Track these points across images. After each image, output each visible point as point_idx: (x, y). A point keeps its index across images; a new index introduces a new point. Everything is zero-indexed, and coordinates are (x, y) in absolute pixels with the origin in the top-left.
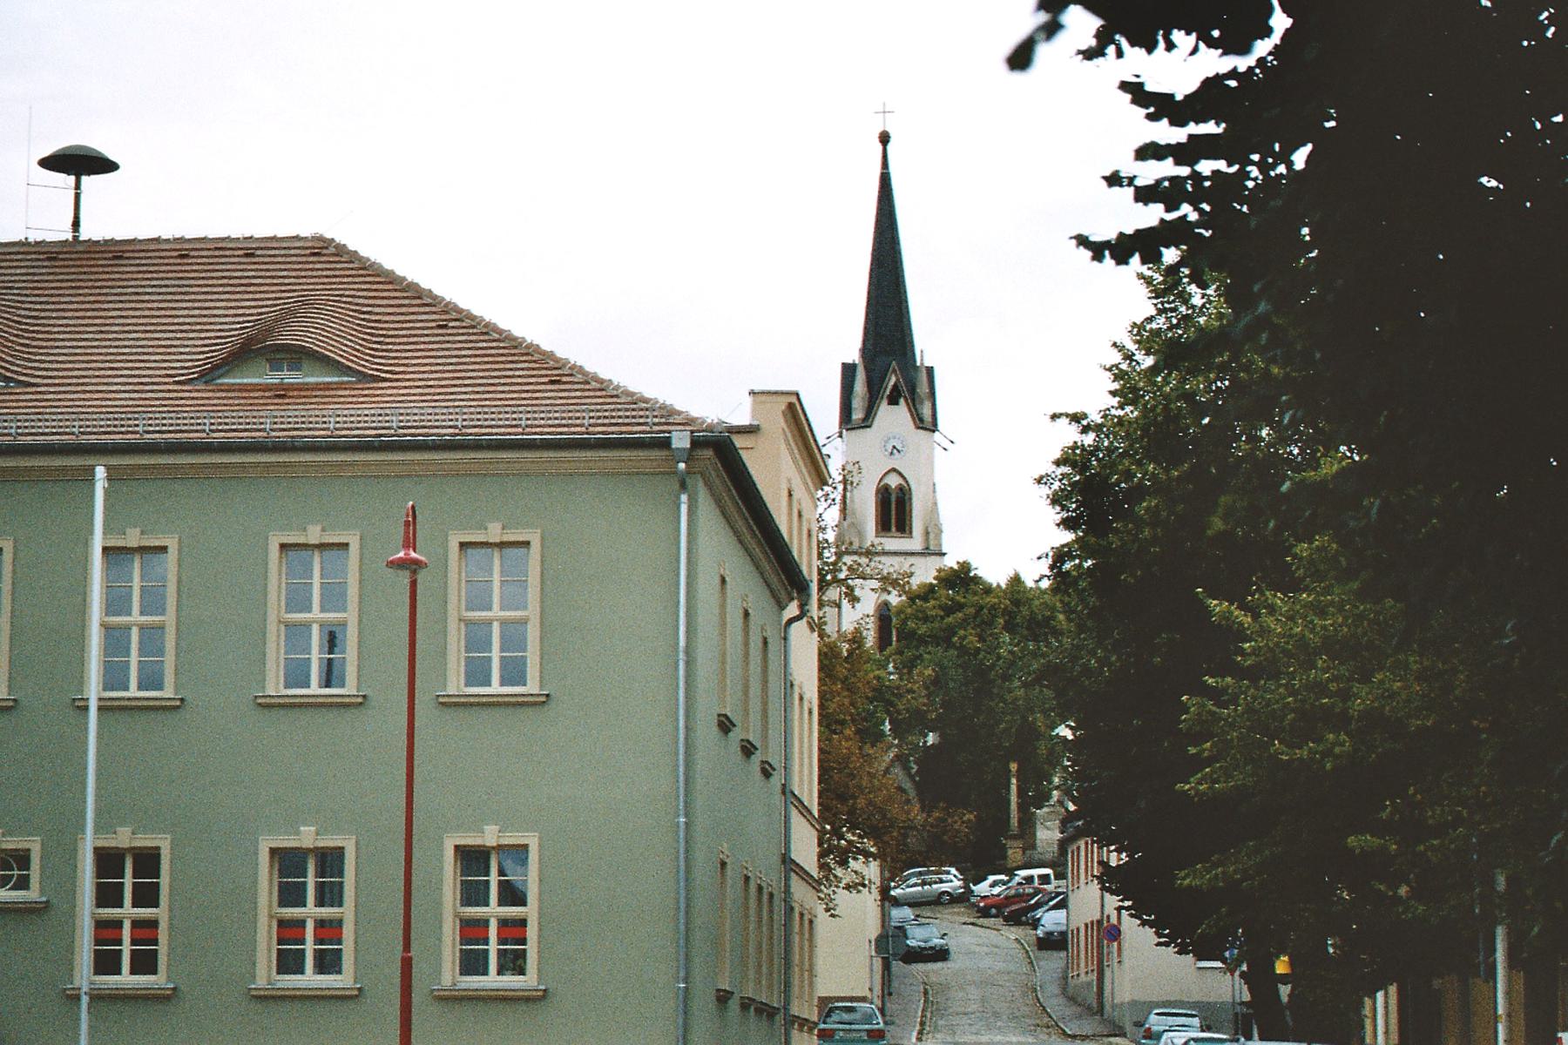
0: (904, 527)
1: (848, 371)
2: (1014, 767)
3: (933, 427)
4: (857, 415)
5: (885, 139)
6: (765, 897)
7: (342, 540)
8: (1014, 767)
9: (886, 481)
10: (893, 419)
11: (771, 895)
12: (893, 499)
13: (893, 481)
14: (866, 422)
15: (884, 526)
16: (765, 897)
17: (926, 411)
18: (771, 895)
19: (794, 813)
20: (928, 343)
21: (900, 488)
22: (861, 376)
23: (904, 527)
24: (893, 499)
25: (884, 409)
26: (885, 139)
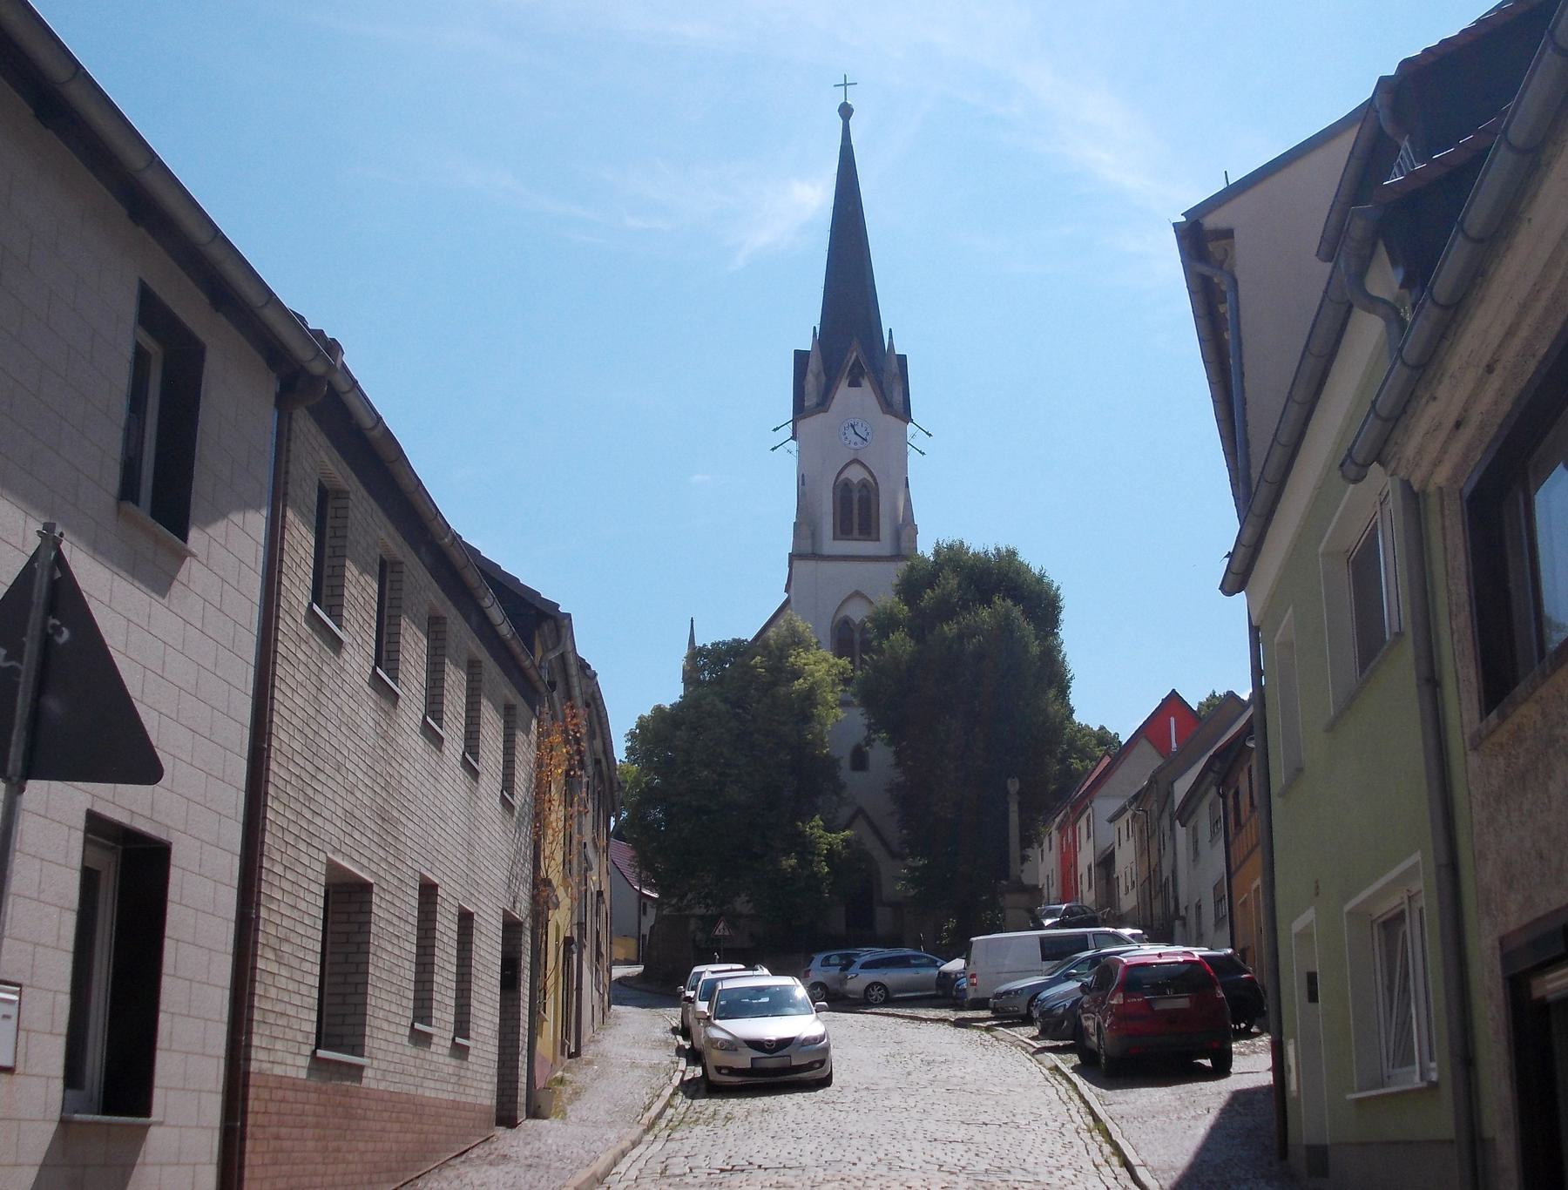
0: (868, 529)
1: (801, 358)
2: (1013, 785)
3: (906, 416)
4: (810, 401)
5: (846, 111)
6: (446, 927)
7: (314, 904)
8: (1013, 785)
9: (847, 474)
10: (854, 400)
11: (466, 920)
12: (856, 496)
13: (856, 475)
14: (823, 404)
15: (844, 529)
16: (446, 927)
17: (897, 397)
18: (466, 920)
19: (304, 423)
20: (901, 320)
21: (864, 484)
22: (814, 365)
23: (868, 529)
24: (856, 496)
25: (844, 392)
26: (846, 111)
